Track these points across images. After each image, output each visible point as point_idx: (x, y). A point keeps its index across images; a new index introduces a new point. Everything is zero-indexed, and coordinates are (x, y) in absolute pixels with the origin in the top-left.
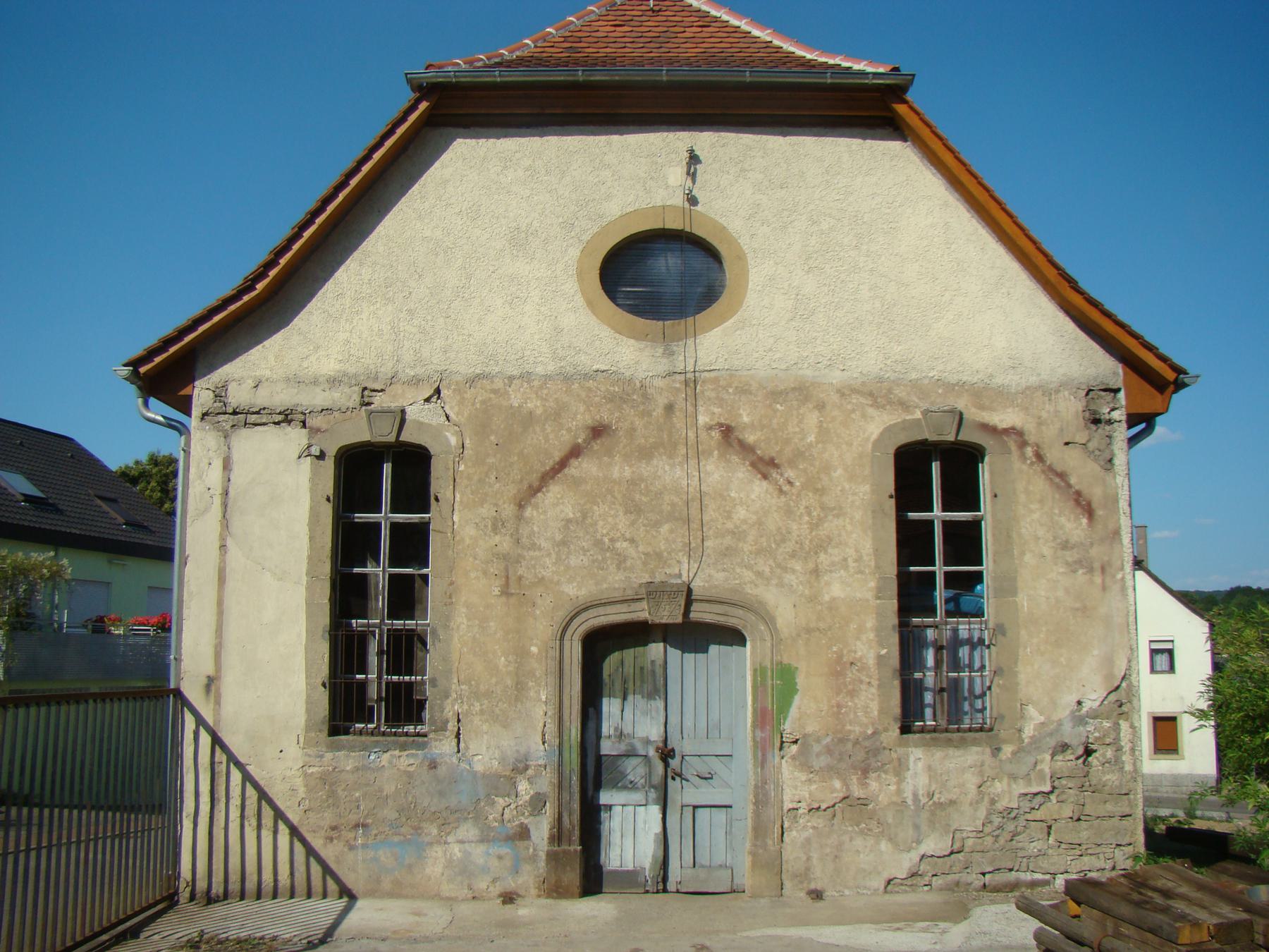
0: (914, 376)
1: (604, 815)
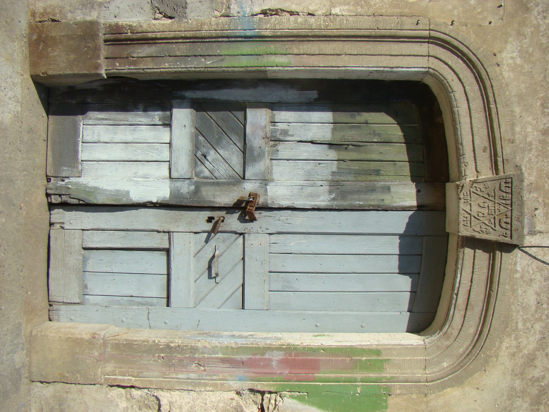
1: (156, 116)
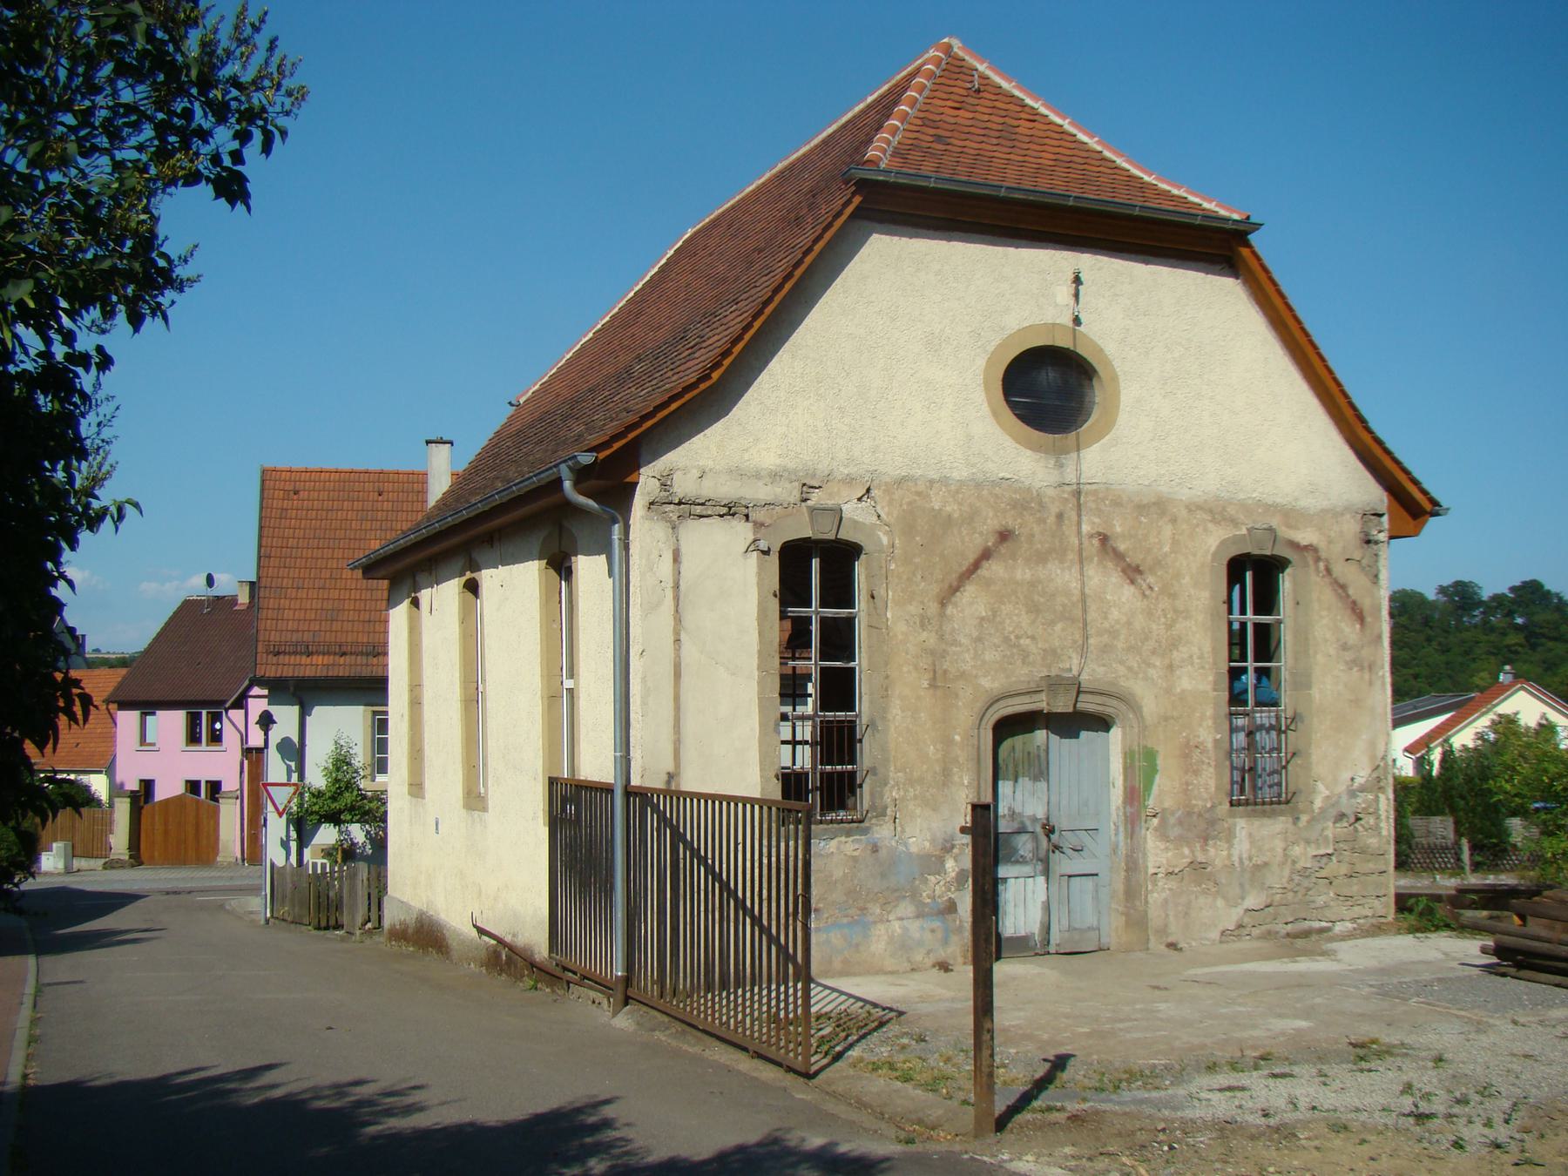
0: (1242, 496)
1: (1001, 887)
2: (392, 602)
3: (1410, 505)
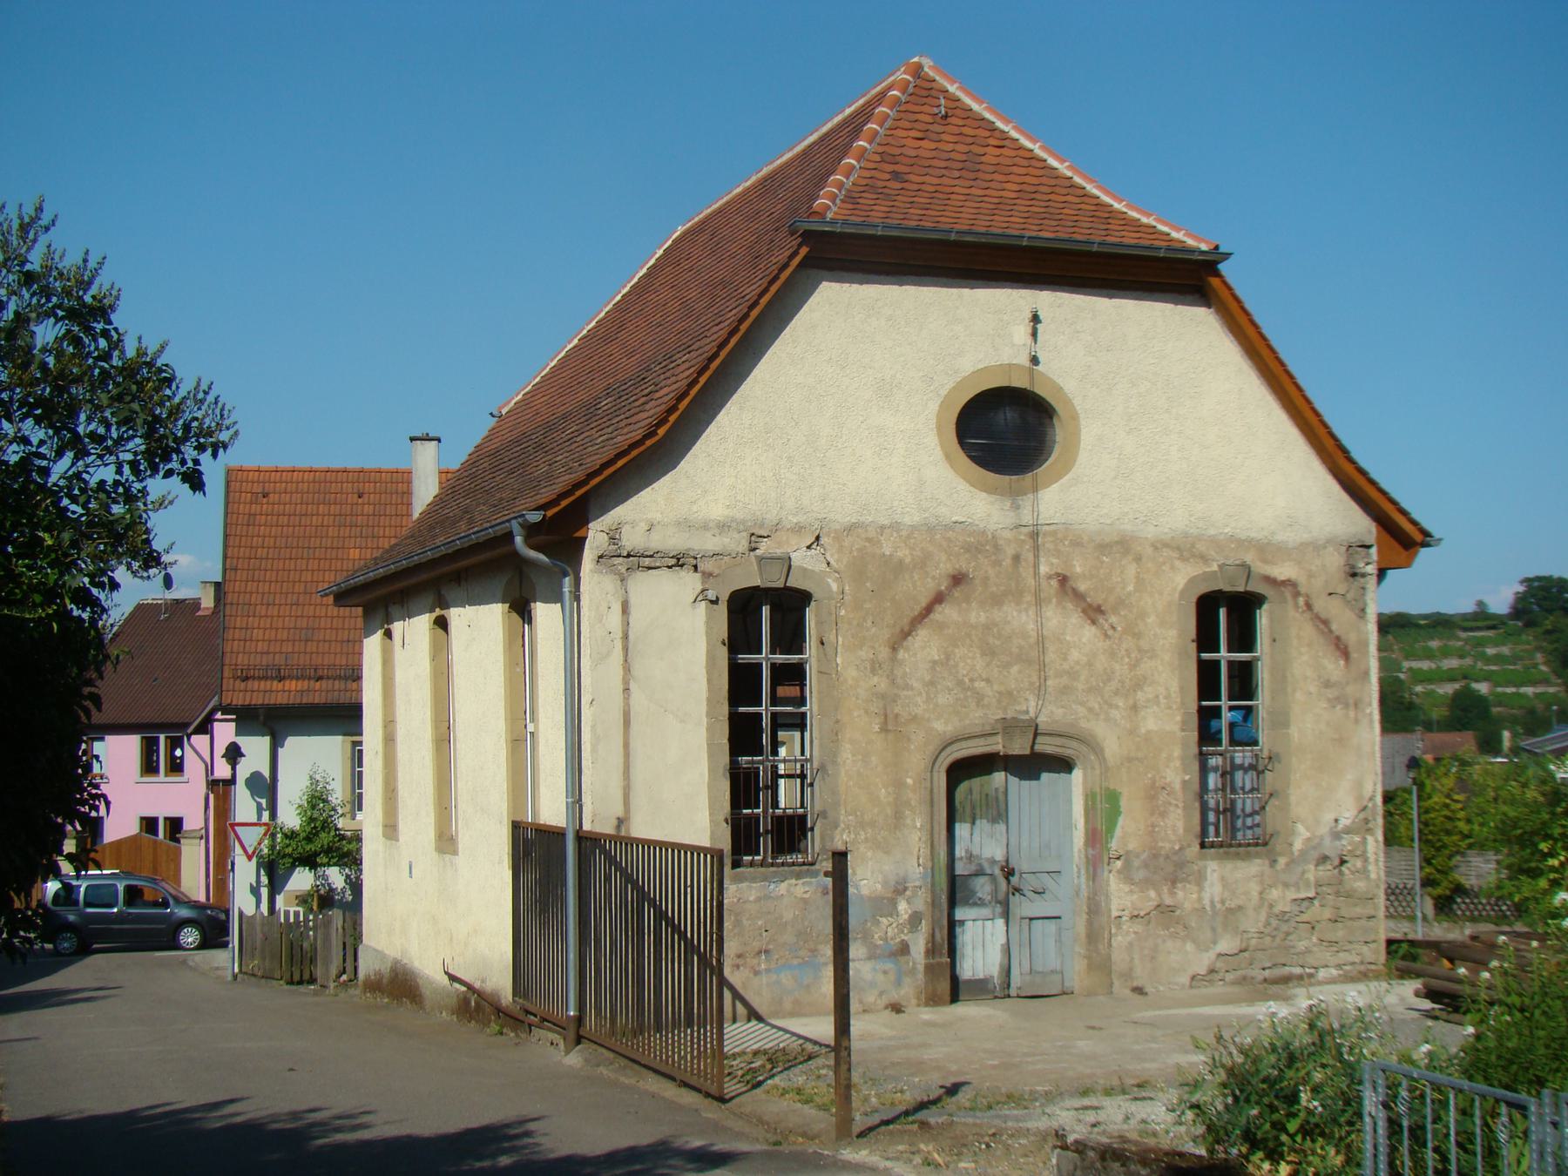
0: (1212, 532)
1: (958, 930)
2: (369, 633)
3: (1400, 536)
